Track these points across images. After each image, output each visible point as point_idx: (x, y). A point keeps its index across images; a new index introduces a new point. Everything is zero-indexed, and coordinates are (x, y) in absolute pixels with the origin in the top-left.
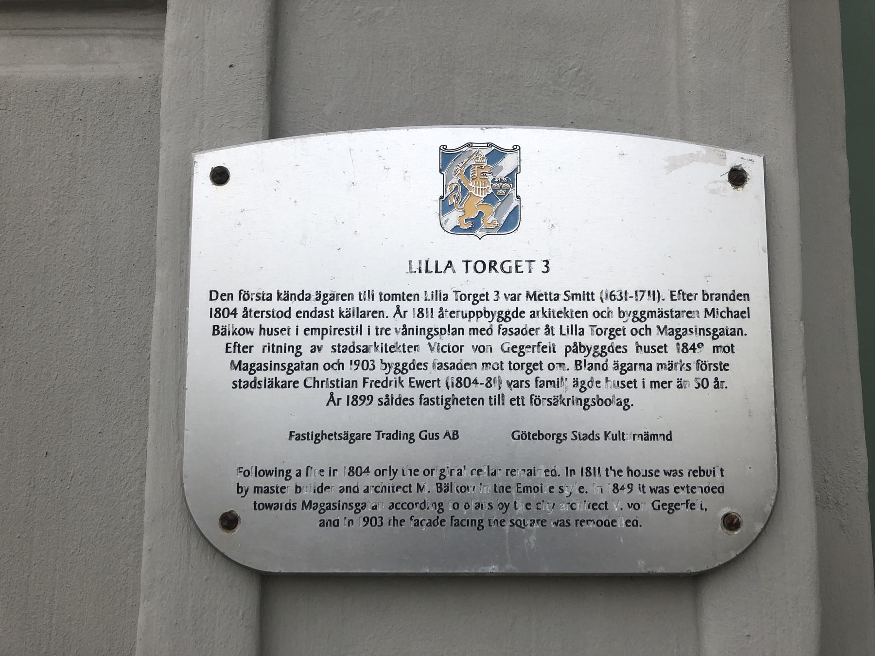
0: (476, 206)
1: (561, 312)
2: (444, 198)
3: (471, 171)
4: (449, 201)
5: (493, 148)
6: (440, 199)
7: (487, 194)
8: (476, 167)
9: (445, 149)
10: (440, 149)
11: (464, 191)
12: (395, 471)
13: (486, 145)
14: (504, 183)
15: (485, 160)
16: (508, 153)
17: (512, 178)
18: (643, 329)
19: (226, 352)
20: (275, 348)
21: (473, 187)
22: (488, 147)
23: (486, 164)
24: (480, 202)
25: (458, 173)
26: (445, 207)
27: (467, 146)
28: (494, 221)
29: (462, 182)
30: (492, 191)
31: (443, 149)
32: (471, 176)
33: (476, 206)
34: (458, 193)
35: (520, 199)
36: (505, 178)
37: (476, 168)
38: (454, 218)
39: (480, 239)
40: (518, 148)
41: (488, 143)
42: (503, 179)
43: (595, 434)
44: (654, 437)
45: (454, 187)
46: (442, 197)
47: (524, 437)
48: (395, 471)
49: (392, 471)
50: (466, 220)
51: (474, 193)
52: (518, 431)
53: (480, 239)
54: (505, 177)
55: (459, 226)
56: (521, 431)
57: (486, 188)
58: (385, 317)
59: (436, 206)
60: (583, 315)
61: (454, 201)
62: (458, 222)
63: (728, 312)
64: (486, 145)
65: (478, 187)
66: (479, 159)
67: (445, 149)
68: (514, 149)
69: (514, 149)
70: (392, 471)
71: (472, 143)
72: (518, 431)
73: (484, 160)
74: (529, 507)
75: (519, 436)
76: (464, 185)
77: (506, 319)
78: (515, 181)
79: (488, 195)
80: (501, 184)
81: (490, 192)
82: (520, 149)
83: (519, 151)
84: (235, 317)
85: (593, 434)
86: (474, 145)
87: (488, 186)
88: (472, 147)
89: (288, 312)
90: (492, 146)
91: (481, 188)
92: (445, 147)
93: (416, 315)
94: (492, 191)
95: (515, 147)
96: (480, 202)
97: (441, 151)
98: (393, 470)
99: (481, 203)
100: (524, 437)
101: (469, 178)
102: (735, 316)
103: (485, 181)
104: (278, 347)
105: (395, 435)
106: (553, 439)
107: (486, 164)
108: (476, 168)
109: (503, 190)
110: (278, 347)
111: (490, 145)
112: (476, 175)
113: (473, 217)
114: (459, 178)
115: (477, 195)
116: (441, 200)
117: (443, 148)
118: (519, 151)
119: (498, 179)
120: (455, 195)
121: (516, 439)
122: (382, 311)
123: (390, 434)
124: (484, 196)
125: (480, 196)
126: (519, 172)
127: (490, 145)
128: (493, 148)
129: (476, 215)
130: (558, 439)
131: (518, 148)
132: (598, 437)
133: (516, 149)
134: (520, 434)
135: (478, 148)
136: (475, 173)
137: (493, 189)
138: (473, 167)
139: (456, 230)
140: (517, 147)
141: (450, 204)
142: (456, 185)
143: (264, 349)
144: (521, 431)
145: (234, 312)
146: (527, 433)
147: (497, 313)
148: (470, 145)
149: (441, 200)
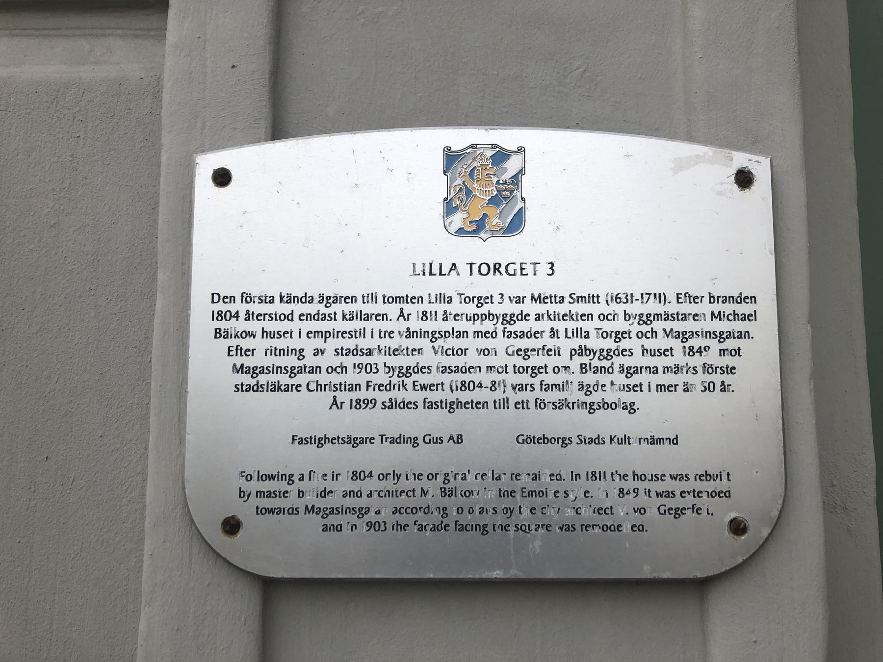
0: (480, 208)
1: (566, 314)
2: (448, 200)
3: (475, 172)
4: (453, 203)
5: (498, 149)
6: (444, 201)
7: (491, 195)
8: (480, 169)
9: (449, 150)
10: (444, 150)
11: (469, 192)
12: (399, 475)
13: (490, 146)
14: (509, 185)
15: (490, 162)
16: (513, 154)
17: (516, 179)
18: (649, 332)
19: (228, 356)
20: (278, 352)
21: (478, 189)
22: (492, 148)
23: (490, 166)
24: (484, 204)
25: (462, 175)
26: (449, 209)
27: (472, 147)
28: (499, 224)
29: (466, 184)
30: (496, 192)
31: (447, 150)
32: (475, 178)
33: (480, 208)
34: (463, 195)
35: (525, 201)
36: (510, 180)
37: (480, 170)
38: (458, 220)
39: (484, 241)
40: (523, 149)
41: (492, 145)
42: (508, 180)
43: (600, 438)
44: (660, 441)
45: (458, 189)
46: (446, 199)
47: (529, 441)
48: (399, 475)
49: (395, 475)
50: (471, 222)
51: (478, 194)
52: (523, 435)
53: (484, 241)
54: (509, 179)
55: (463, 228)
56: (525, 435)
57: (491, 189)
58: (389, 319)
59: (440, 208)
60: (588, 318)
61: (458, 203)
62: (462, 224)
63: (735, 314)
64: (490, 146)
65: (482, 189)
66: (483, 160)
67: (449, 150)
68: (519, 150)
69: (519, 150)
70: (395, 475)
71: (476, 145)
72: (523, 435)
73: (489, 162)
74: (533, 512)
75: (523, 440)
76: (468, 186)
77: (510, 321)
78: (520, 183)
79: (492, 196)
80: (506, 186)
81: (495, 194)
82: (524, 150)
83: (523, 152)
84: (237, 320)
85: (598, 438)
86: (478, 146)
87: (492, 188)
88: (476, 148)
89: (291, 315)
90: (497, 147)
91: (485, 189)
92: (449, 148)
93: (420, 318)
94: (496, 192)
95: (520, 148)
96: (484, 204)
97: (445, 152)
98: (397, 474)
99: (485, 205)
100: (529, 441)
101: (473, 179)
102: (742, 319)
103: (490, 182)
104: (280, 350)
105: (399, 439)
106: (558, 443)
107: (490, 166)
108: (480, 170)
109: (508, 191)
110: (280, 350)
111: (494, 146)
112: (480, 176)
113: (477, 219)
114: (463, 180)
115: (481, 197)
116: (445, 202)
117: (447, 149)
118: (523, 152)
119: (503, 180)
120: (460, 197)
121: (521, 443)
122: (386, 314)
123: (394, 438)
124: (488, 198)
125: (485, 197)
126: (523, 173)
127: (494, 146)
128: (498, 149)
129: (481, 217)
130: (563, 443)
131: (523, 149)
132: (604, 441)
133: (521, 150)
134: (525, 438)
135: (483, 149)
136: (479, 175)
137: (497, 191)
138: (477, 168)
139: (460, 232)
140: (521, 149)
141: (454, 206)
142: (460, 186)
143: (266, 352)
144: (525, 435)
145: (236, 315)
146: (532, 437)
147: (501, 315)
148: (474, 146)
149: (445, 202)
